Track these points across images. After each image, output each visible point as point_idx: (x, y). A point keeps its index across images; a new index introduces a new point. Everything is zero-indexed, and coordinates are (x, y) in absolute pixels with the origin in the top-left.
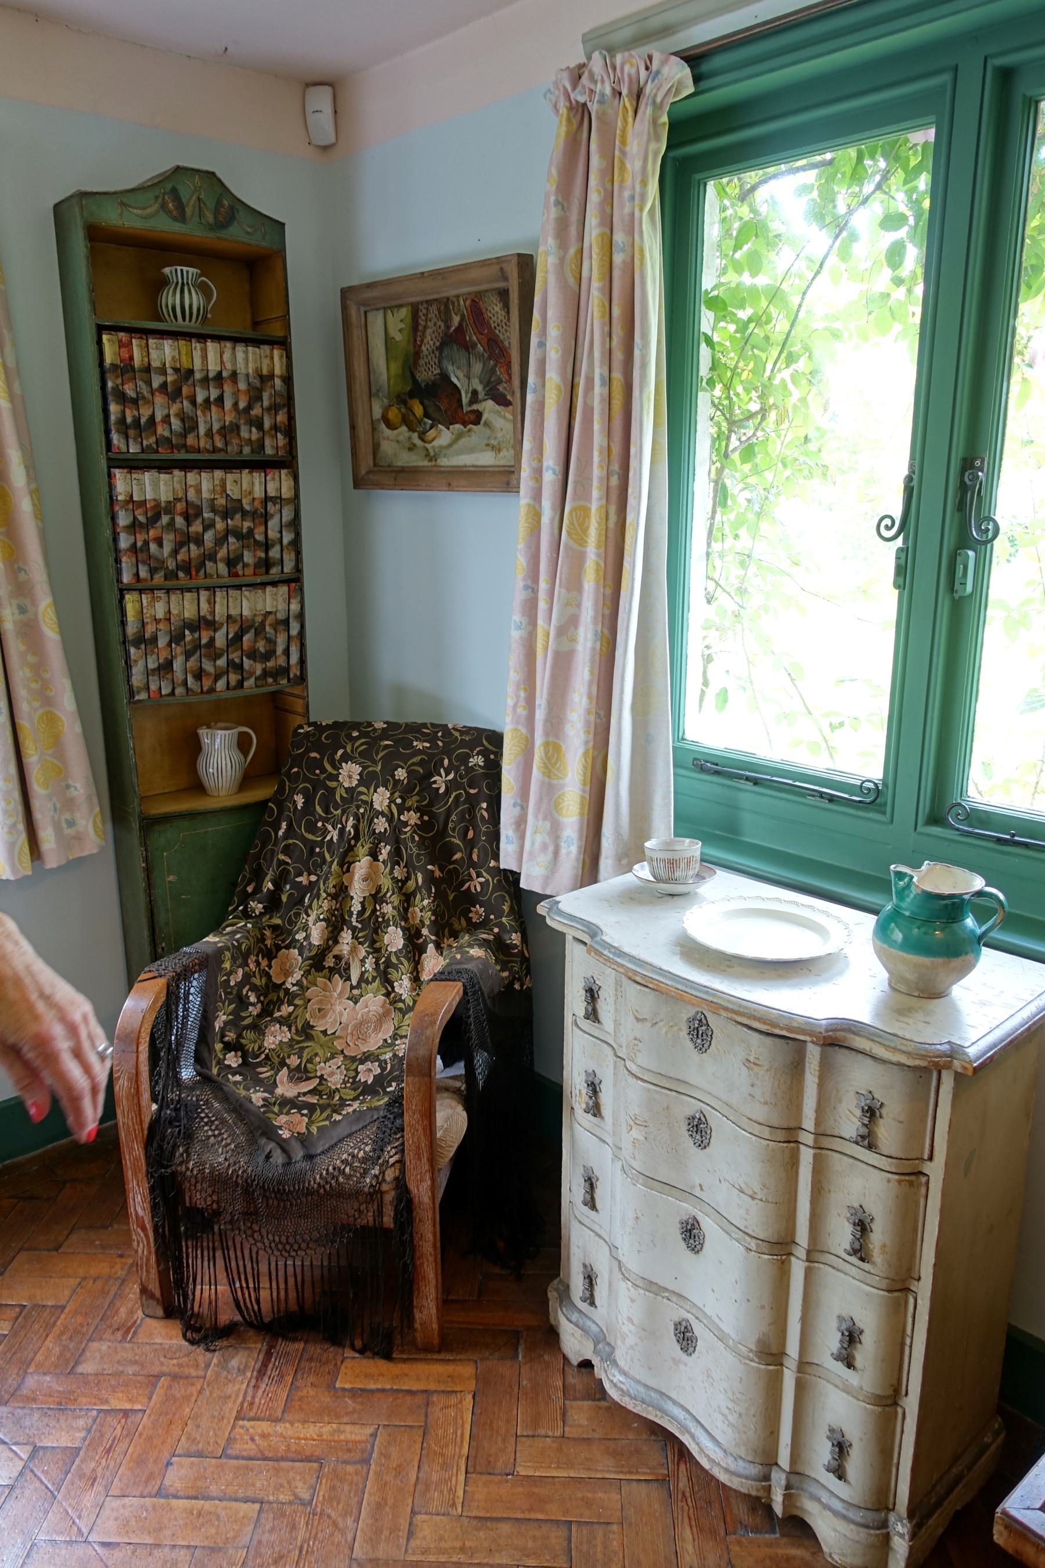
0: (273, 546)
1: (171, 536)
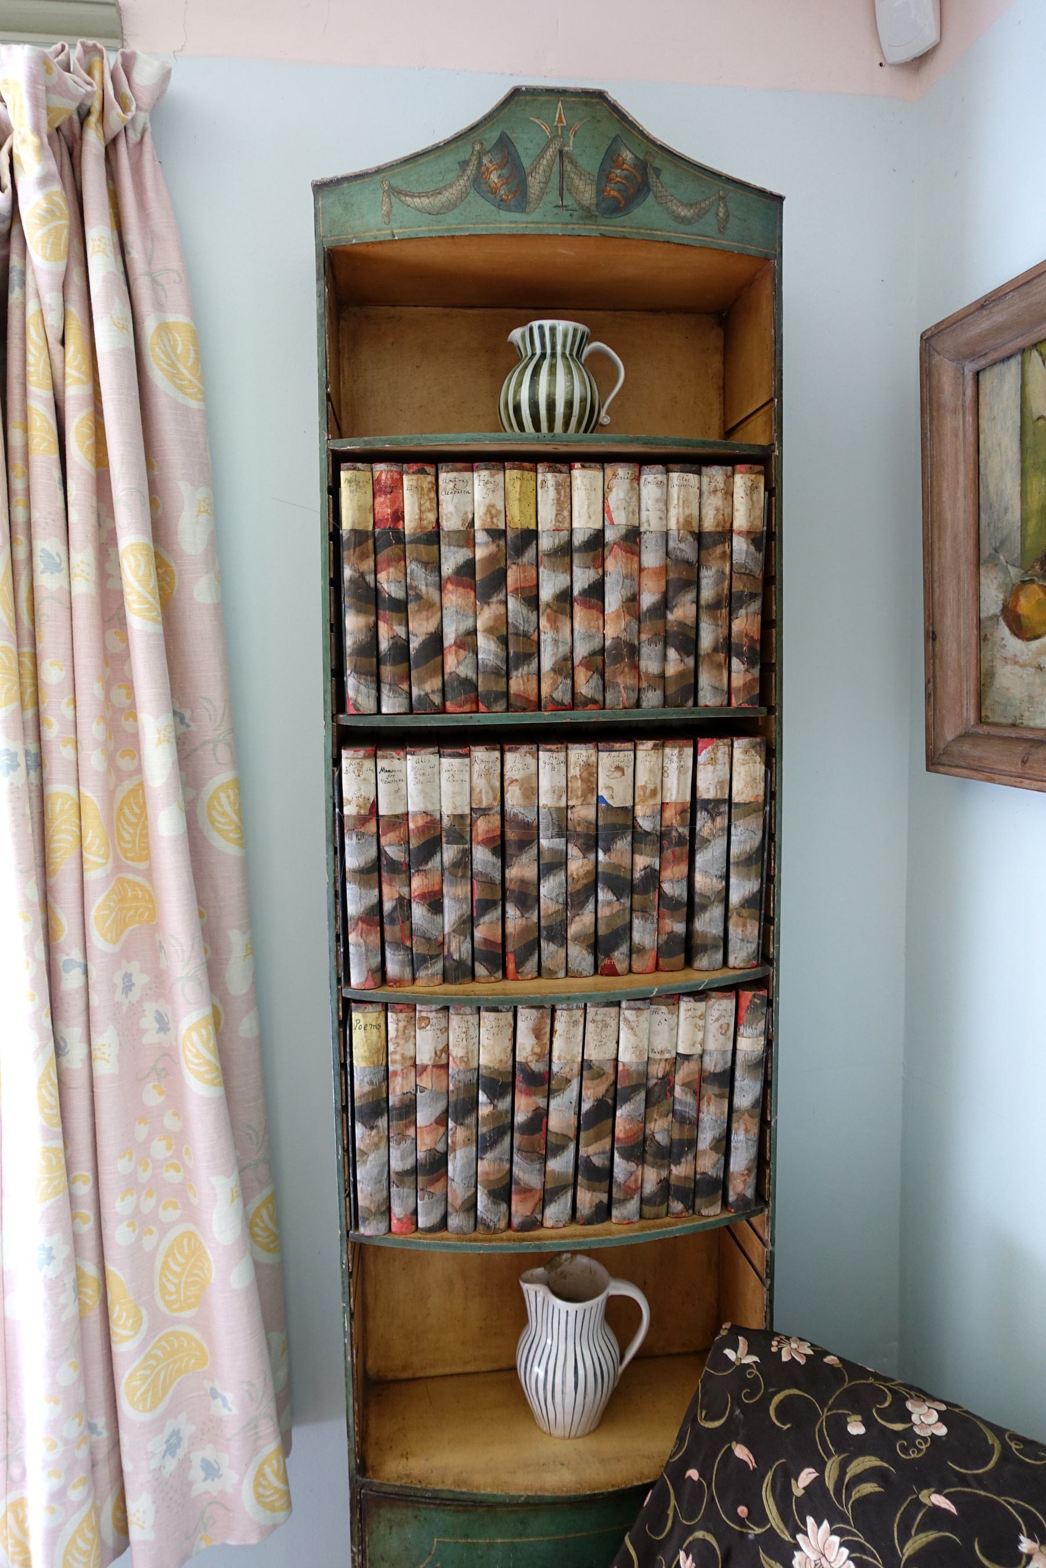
0: (704, 908)
1: (462, 890)
